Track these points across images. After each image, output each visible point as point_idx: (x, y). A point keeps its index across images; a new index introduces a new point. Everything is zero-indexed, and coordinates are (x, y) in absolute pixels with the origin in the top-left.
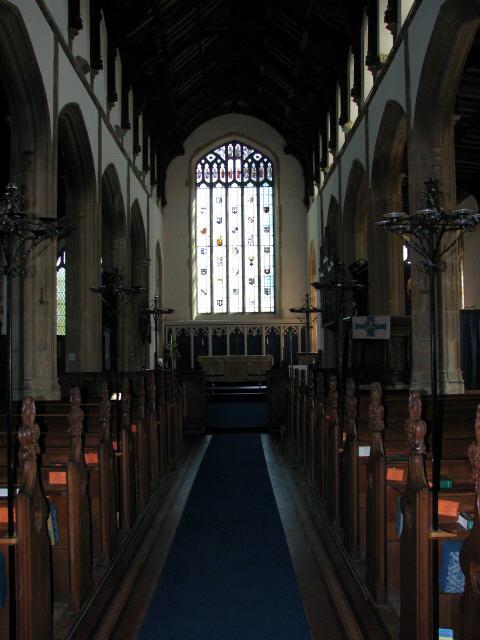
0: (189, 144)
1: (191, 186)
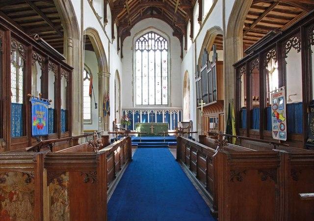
0: (133, 31)
1: (133, 49)
